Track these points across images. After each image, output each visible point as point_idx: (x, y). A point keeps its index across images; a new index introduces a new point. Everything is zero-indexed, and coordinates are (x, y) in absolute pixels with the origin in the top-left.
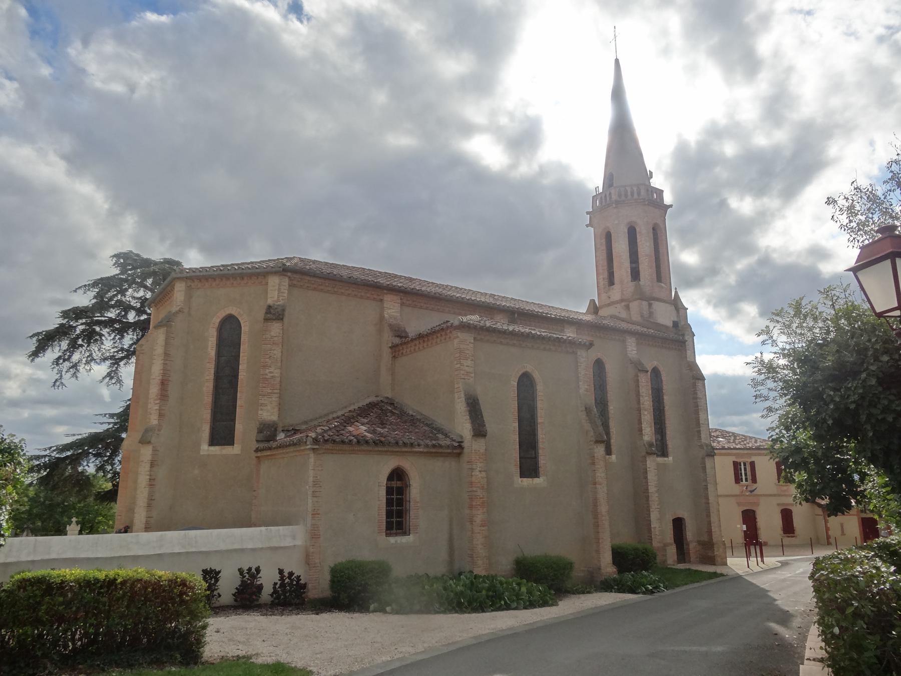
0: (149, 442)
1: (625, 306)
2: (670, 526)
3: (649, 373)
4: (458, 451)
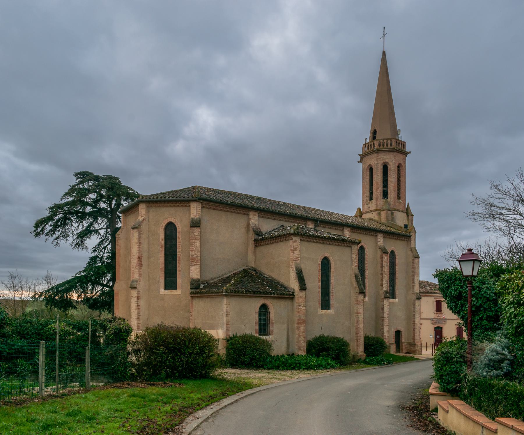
0: (136, 288)
1: (378, 213)
2: (393, 334)
3: (389, 254)
4: (292, 296)
